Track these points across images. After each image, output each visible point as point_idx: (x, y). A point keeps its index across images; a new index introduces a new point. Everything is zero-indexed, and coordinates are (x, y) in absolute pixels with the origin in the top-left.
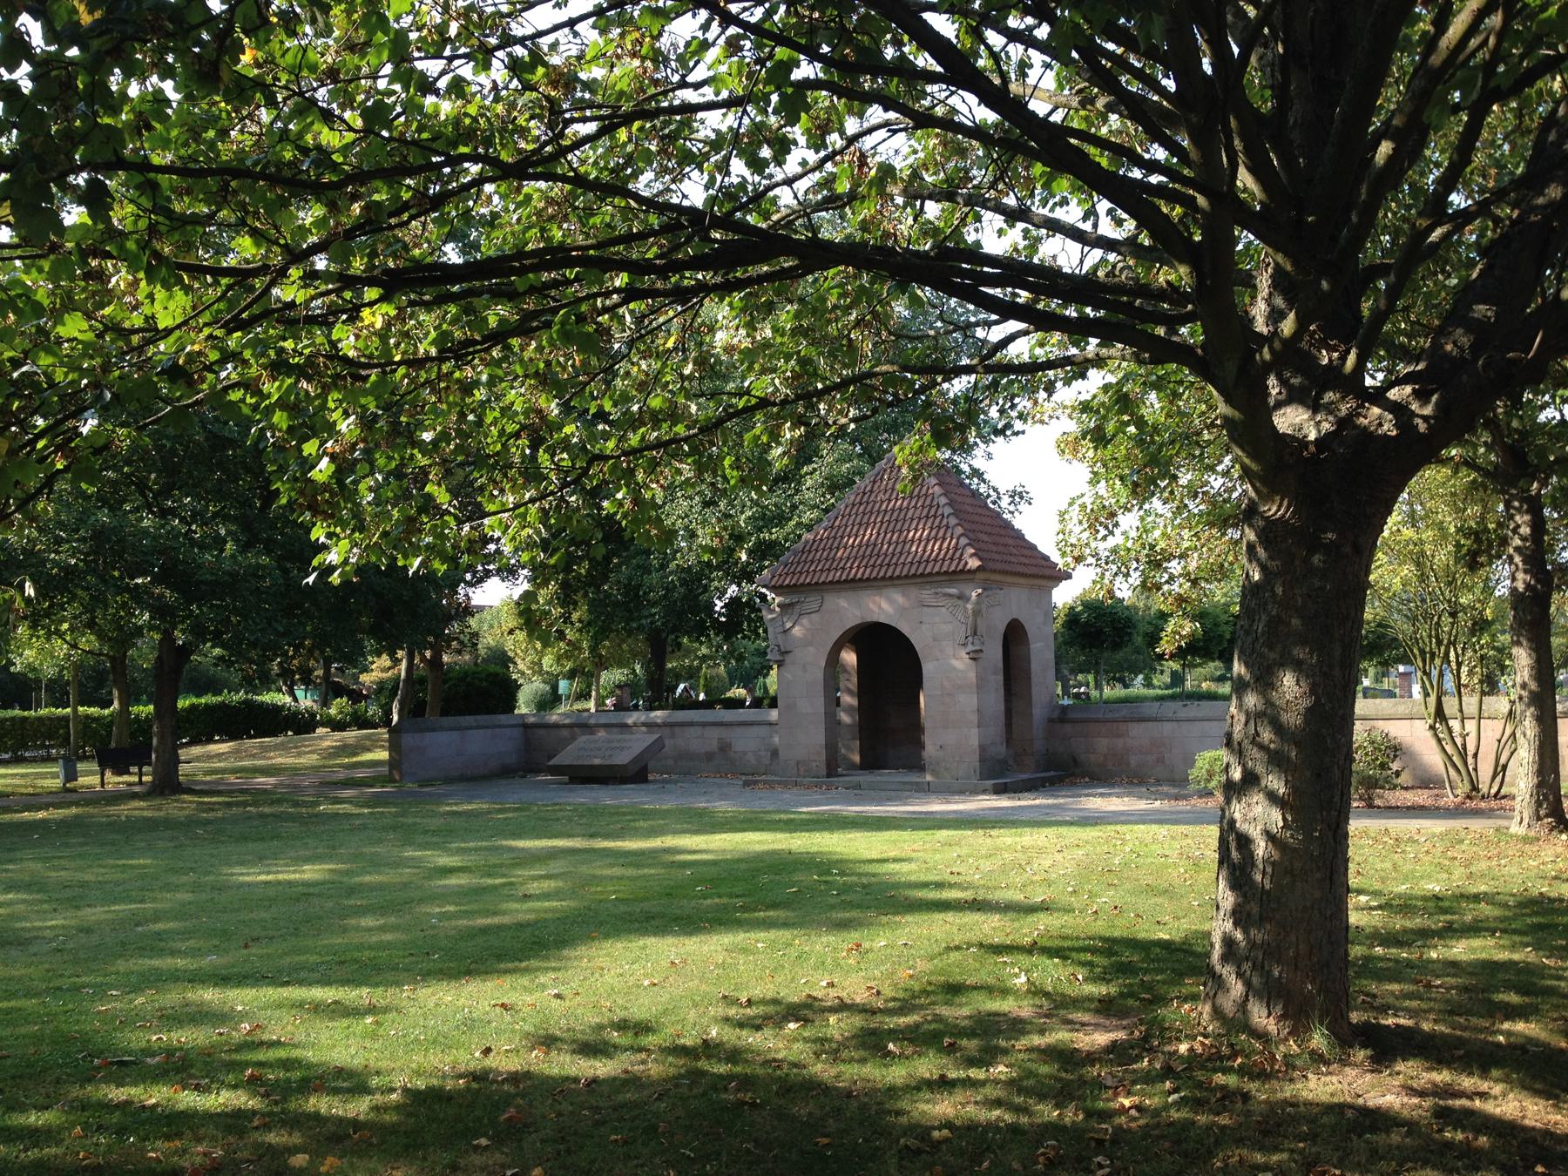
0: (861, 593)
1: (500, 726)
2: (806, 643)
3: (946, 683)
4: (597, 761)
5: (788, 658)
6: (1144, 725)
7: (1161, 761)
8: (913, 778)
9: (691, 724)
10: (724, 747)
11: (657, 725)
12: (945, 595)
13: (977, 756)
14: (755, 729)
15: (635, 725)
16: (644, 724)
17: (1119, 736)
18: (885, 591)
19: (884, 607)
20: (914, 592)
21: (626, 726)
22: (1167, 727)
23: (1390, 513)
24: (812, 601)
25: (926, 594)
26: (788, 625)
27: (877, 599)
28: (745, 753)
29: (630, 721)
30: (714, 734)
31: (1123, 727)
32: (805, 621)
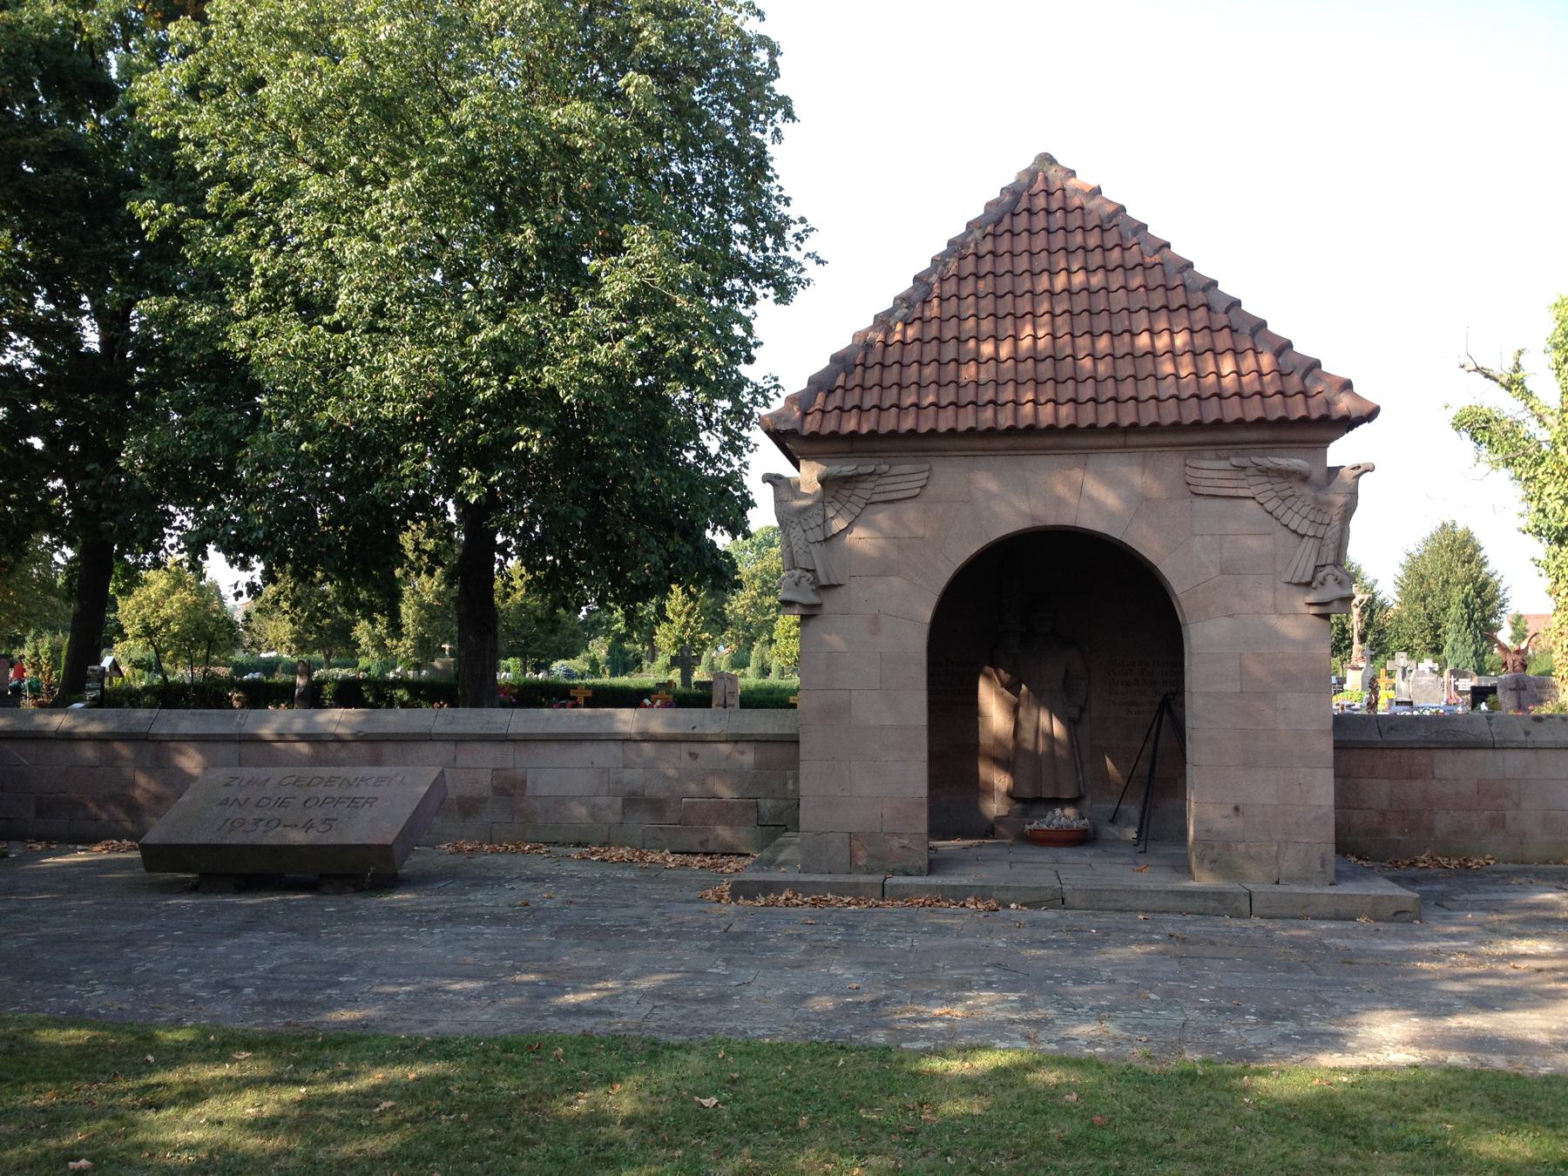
0: (1032, 462)
1: (477, 918)
2: (882, 568)
3: (1255, 668)
4: (297, 837)
5: (831, 601)
6: (1465, 754)
7: (1498, 823)
8: (1152, 878)
9: (427, 738)
10: (508, 789)
11: (338, 739)
12: (1265, 472)
13: (1330, 832)
14: (589, 752)
15: (281, 737)
16: (303, 738)
17: (1412, 776)
18: (1094, 460)
19: (1093, 495)
20: (1172, 464)
21: (256, 740)
22: (1512, 761)
23: (494, 580)
24: (905, 473)
25: (1211, 469)
26: (838, 524)
27: (1077, 474)
28: (560, 801)
29: (266, 731)
30: (488, 757)
31: (1421, 758)
32: (882, 517)
